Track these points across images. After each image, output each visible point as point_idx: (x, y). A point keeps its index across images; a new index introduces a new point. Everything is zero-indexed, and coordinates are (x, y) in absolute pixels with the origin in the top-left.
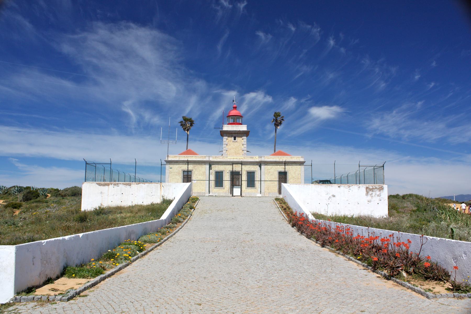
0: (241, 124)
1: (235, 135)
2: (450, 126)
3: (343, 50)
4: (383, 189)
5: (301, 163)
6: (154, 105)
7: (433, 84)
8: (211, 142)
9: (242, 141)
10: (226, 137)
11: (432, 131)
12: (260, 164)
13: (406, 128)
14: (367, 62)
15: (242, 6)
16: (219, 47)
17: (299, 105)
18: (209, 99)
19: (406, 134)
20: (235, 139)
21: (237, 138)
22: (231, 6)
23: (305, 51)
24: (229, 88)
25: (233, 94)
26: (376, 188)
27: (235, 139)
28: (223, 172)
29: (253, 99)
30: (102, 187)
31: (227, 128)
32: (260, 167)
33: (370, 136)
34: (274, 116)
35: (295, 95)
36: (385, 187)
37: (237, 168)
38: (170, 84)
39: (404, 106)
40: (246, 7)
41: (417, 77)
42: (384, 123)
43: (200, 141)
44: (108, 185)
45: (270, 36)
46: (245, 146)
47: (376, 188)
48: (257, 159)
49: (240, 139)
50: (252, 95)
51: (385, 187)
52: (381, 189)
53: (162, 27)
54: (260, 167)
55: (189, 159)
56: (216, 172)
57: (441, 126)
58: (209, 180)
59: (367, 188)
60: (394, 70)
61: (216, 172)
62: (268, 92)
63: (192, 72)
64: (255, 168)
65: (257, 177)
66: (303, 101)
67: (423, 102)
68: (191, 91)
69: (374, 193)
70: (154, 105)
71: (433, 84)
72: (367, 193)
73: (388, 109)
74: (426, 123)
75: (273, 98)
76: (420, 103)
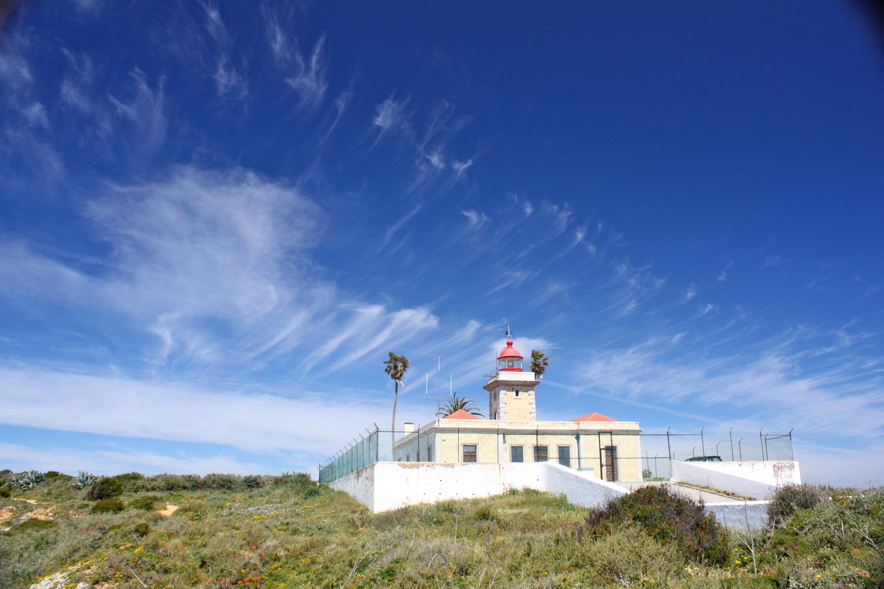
0: (521, 370)
1: (517, 387)
2: (710, 374)
3: (592, 248)
4: (793, 467)
5: (635, 433)
6: (219, 327)
7: (710, 307)
8: (290, 397)
9: (528, 398)
10: (505, 392)
11: (678, 383)
12: (577, 435)
13: (640, 379)
14: (623, 269)
15: (461, 167)
16: (390, 232)
17: (479, 337)
18: (329, 318)
19: (637, 388)
20: (517, 395)
21: (520, 393)
22: (441, 166)
23: (532, 246)
24: (372, 299)
25: (375, 310)
26: (785, 466)
27: (517, 395)
28: (522, 447)
29: (406, 321)
30: (407, 469)
31: (504, 376)
32: (578, 438)
33: (577, 390)
34: (533, 356)
35: (477, 317)
36: (796, 464)
37: (543, 441)
38: (271, 288)
39: (652, 341)
40: (469, 170)
41: (690, 295)
42: (609, 370)
43: (272, 394)
44: (418, 467)
45: (485, 218)
46: (534, 406)
47: (785, 466)
48: (572, 426)
49: (526, 394)
50: (406, 314)
51: (796, 464)
52: (792, 467)
53: (309, 190)
54: (578, 438)
55: (462, 426)
56: (512, 447)
57: (696, 374)
58: (579, 458)
59: (774, 466)
60: (659, 283)
61: (512, 447)
62: (436, 312)
63: (319, 267)
64: (569, 441)
65: (573, 453)
66: (489, 328)
67: (683, 335)
68: (301, 302)
69: (783, 473)
70: (219, 327)
71: (710, 307)
72: (775, 472)
73: (621, 345)
74: (673, 370)
75: (439, 322)
76: (678, 336)
